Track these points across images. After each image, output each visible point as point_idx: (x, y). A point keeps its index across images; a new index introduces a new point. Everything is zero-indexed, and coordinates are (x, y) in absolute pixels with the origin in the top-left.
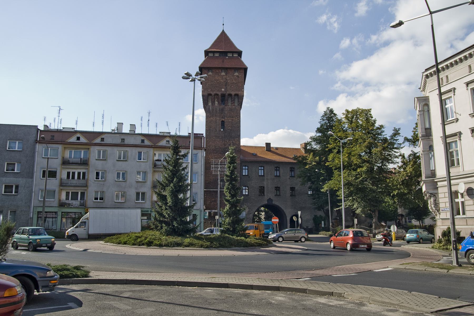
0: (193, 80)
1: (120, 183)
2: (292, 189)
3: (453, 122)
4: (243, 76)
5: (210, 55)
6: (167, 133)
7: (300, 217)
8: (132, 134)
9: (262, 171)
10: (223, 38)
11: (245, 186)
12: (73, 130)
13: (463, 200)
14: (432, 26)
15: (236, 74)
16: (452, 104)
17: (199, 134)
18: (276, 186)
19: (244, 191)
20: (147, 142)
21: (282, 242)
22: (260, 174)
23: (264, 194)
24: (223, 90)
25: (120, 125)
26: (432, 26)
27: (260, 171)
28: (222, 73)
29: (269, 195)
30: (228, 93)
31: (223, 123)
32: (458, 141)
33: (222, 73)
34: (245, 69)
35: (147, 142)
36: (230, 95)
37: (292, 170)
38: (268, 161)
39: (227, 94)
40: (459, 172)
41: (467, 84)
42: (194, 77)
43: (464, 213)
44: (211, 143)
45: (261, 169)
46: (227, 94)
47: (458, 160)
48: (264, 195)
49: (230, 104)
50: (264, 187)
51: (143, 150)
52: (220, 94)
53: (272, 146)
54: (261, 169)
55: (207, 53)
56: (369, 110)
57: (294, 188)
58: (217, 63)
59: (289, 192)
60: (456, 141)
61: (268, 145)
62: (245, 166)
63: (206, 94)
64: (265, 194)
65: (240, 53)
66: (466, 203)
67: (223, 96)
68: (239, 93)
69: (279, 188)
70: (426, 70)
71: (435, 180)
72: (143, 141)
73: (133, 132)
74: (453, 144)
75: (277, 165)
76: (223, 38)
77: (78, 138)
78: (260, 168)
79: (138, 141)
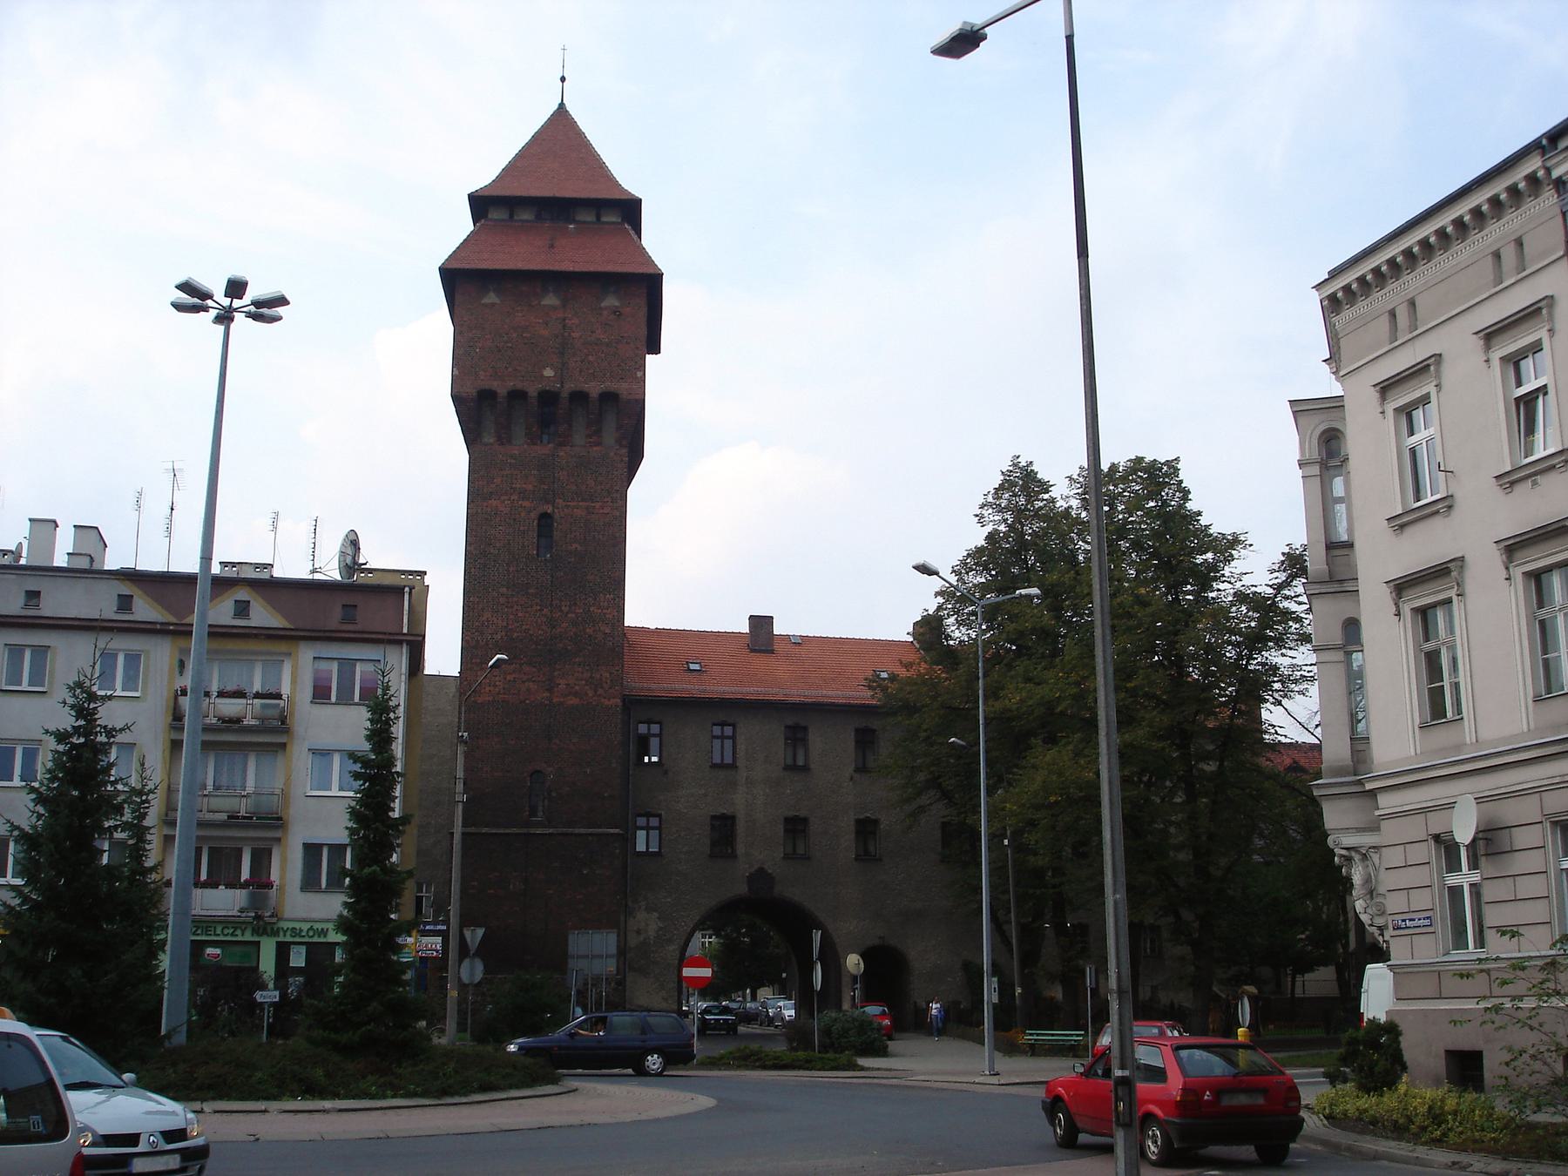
0: (225, 318)
1: (12, 794)
2: (866, 829)
3: (1437, 512)
4: (643, 313)
5: (494, 214)
6: (257, 566)
7: (819, 959)
8: (86, 571)
9: (728, 743)
10: (560, 136)
11: (648, 815)
12: (265, 575)
13: (1453, 880)
14: (1070, 39)
15: (611, 301)
16: (1432, 430)
17: (411, 573)
18: (791, 813)
19: (641, 835)
20: (145, 610)
21: (660, 1075)
22: (717, 760)
23: (734, 851)
24: (548, 372)
25: (44, 527)
26: (1070, 39)
27: (717, 743)
28: (554, 305)
29: (759, 850)
30: (570, 386)
31: (545, 519)
32: (1455, 599)
33: (554, 305)
34: (651, 284)
35: (145, 610)
36: (579, 397)
37: (865, 740)
38: (759, 694)
39: (565, 394)
40: (1459, 747)
41: (1490, 336)
42: (226, 302)
43: (1481, 942)
44: (487, 615)
45: (722, 737)
46: (565, 394)
47: (1456, 686)
48: (734, 856)
49: (579, 438)
50: (733, 818)
51: (122, 644)
52: (533, 391)
53: (778, 629)
54: (722, 737)
55: (480, 204)
56: (1172, 466)
57: (876, 822)
58: (523, 252)
59: (847, 842)
60: (1449, 601)
61: (761, 624)
62: (649, 722)
63: (470, 390)
64: (741, 849)
65: (630, 210)
66: (1489, 893)
67: (548, 398)
68: (622, 388)
69: (805, 820)
70: (1335, 274)
71: (1369, 786)
72: (125, 603)
73: (83, 563)
74: (1440, 614)
75: (797, 720)
76: (560, 136)
77: (242, 609)
78: (717, 730)
79: (99, 603)
